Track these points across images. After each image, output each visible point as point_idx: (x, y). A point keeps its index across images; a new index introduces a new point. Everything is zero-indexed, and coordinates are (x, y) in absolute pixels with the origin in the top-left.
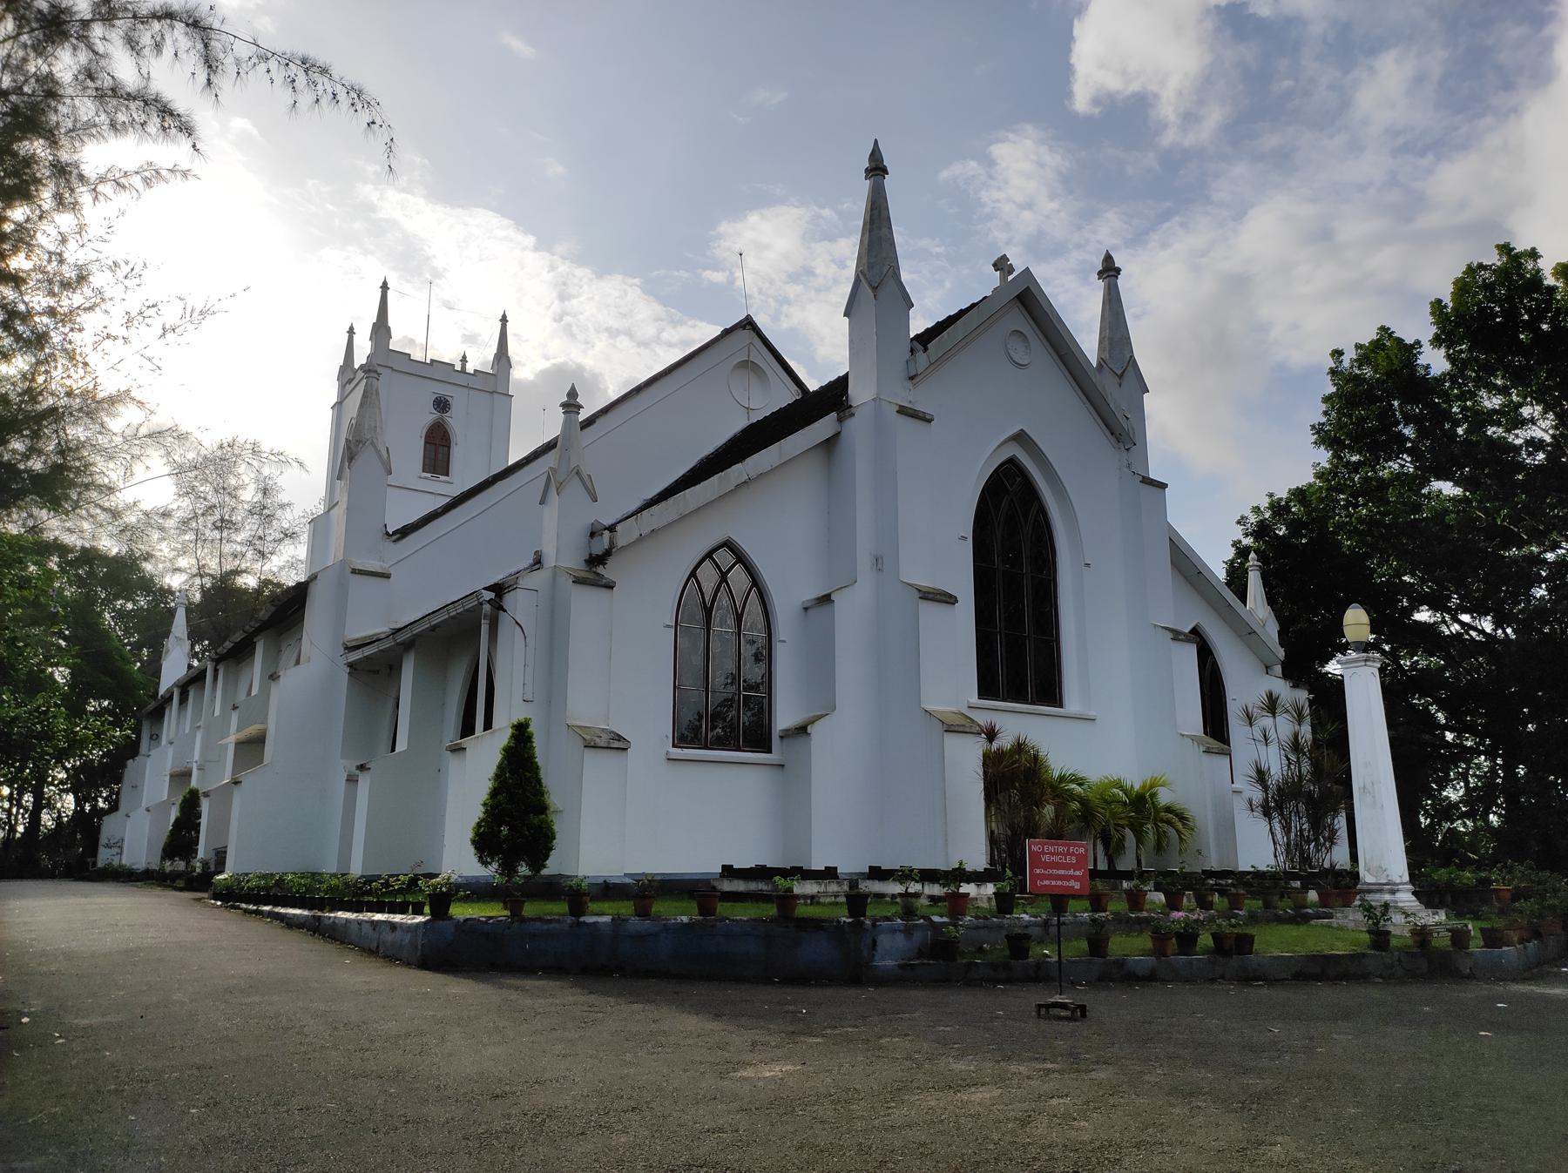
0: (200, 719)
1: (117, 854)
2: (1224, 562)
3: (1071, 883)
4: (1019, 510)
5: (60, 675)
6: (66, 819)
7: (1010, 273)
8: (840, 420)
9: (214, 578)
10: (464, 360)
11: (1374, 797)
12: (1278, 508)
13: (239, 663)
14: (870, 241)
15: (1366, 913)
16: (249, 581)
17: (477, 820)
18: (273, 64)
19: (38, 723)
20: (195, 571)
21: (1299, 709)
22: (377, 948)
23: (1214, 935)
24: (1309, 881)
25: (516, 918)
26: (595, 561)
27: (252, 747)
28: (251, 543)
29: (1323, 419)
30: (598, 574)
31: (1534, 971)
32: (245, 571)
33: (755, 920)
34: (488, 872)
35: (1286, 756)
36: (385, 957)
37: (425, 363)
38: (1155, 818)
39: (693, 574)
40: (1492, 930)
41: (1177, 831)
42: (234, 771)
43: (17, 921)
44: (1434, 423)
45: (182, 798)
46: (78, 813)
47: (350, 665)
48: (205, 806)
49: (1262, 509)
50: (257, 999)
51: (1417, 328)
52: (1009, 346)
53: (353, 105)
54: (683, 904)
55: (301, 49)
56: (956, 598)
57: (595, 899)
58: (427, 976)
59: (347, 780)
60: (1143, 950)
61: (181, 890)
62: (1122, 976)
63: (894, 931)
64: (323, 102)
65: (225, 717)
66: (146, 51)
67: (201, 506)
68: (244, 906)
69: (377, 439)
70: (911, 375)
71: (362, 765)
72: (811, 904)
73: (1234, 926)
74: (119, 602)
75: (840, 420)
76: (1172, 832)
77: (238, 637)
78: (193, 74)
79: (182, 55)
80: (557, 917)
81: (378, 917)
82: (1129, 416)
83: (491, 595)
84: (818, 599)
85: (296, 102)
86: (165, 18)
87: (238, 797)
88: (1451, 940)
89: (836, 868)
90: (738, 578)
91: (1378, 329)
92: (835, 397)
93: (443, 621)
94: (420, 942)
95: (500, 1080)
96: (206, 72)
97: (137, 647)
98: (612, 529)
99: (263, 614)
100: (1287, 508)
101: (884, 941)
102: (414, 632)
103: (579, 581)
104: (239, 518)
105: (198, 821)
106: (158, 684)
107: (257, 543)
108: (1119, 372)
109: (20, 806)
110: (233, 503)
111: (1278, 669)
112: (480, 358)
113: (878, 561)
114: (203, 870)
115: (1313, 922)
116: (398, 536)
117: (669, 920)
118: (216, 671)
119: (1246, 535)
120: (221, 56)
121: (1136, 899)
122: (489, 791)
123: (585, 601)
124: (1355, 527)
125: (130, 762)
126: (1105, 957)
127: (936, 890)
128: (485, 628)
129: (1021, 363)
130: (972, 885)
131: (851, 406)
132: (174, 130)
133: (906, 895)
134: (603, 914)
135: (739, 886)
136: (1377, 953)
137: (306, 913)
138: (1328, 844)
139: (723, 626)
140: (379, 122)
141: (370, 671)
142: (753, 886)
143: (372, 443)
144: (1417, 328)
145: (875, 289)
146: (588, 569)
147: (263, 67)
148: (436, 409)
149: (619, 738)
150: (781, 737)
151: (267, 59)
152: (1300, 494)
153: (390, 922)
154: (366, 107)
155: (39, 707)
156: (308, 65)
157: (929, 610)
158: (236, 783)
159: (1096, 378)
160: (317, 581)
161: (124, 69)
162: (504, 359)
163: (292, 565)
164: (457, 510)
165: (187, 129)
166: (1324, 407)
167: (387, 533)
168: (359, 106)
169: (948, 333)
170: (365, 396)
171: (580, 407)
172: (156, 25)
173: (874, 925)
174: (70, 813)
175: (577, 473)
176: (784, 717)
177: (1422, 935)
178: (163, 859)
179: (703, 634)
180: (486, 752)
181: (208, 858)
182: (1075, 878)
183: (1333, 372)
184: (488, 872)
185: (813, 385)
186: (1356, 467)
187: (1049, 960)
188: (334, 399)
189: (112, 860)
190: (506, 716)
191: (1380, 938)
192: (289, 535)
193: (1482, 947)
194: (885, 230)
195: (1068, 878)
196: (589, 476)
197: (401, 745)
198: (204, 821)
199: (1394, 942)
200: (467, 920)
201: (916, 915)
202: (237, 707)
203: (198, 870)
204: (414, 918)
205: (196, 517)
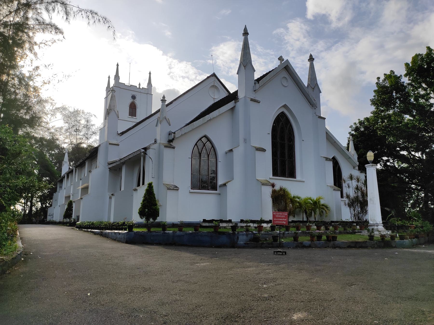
0: (72, 183)
1: (52, 218)
2: (347, 138)
3: (283, 222)
4: (284, 126)
5: (36, 172)
6: (39, 209)
8: (235, 103)
9: (75, 145)
10: (140, 85)
11: (373, 201)
12: (361, 123)
13: (82, 168)
14: (243, 53)
15: (368, 231)
16: (84, 146)
17: (140, 208)
18: (83, 12)
19: (31, 183)
20: (70, 143)
21: (358, 178)
22: (115, 239)
23: (326, 236)
24: (357, 223)
25: (149, 232)
26: (170, 141)
27: (85, 190)
28: (84, 135)
29: (373, 98)
30: (171, 145)
31: (413, 246)
32: (83, 143)
33: (208, 232)
34: (143, 221)
35: (355, 191)
37: (129, 86)
38: (319, 208)
39: (196, 144)
40: (402, 235)
41: (325, 211)
42: (82, 195)
43: (28, 233)
44: (405, 97)
45: (68, 203)
46: (42, 207)
47: (109, 168)
48: (74, 205)
49: (357, 123)
50: (85, 249)
51: (401, 71)
52: (282, 81)
53: (104, 22)
54: (191, 229)
55: (90, 8)
56: (266, 150)
57: (169, 227)
58: (127, 245)
59: (109, 198)
60: (308, 240)
61: (68, 226)
62: (302, 246)
63: (243, 235)
64: (96, 22)
65: (78, 182)
66: (51, 12)
68: (84, 230)
69: (115, 108)
70: (255, 90)
71: (113, 194)
72: (224, 229)
73: (331, 234)
74: (50, 151)
75: (235, 103)
76: (324, 211)
77: (81, 161)
78: (63, 17)
79: (60, 12)
80: (159, 231)
81: (116, 231)
82: (315, 100)
83: (143, 150)
84: (229, 150)
85: (89, 22)
86: (55, 2)
87: (82, 202)
88: (391, 238)
89: (231, 220)
90: (208, 144)
91: (390, 71)
92: (233, 97)
93: (131, 157)
94: (126, 237)
95: (140, 265)
96: (66, 16)
97: (56, 163)
98: (174, 133)
99: (87, 155)
100: (364, 123)
101: (241, 237)
102: (125, 160)
103: (166, 147)
104: (81, 129)
105: (72, 209)
106: (61, 173)
107: (86, 135)
108: (313, 87)
109: (27, 205)
110: (79, 124)
111: (357, 168)
112: (144, 85)
113: (245, 140)
114: (74, 221)
115: (356, 234)
116: (121, 134)
117: (187, 232)
118: (76, 170)
119: (352, 131)
120: (70, 11)
121: (308, 228)
122: (142, 200)
123: (167, 152)
124: (381, 128)
125: (54, 194)
126: (298, 241)
127: (256, 225)
129: (285, 86)
131: (238, 99)
132: (59, 33)
133: (247, 226)
134: (171, 231)
135: (207, 224)
136: (370, 241)
137: (99, 231)
138: (365, 214)
139: (204, 157)
140: (111, 26)
141: (114, 170)
142: (210, 224)
143: (114, 110)
144: (401, 71)
145: (245, 67)
146: (168, 143)
147: (80, 13)
148: (135, 96)
149: (176, 187)
150: (220, 187)
151: (82, 11)
152: (367, 119)
154: (107, 22)
155: (32, 180)
156: (92, 12)
157: (258, 153)
158: (81, 199)
161: (45, 16)
162: (150, 84)
163: (95, 141)
164: (136, 127)
165: (62, 33)
166: (374, 94)
167: (118, 134)
168: (106, 22)
169: (265, 78)
170: (112, 97)
171: (166, 101)
172: (53, 4)
173: (238, 233)
174: (40, 207)
175: (165, 118)
176: (220, 182)
177: (383, 237)
178: (64, 219)
179: (199, 160)
180: (142, 191)
181: (75, 218)
183: (377, 83)
184: (143, 221)
186: (382, 111)
187: (283, 242)
188: (105, 96)
189: (51, 219)
190: (146, 183)
191: (371, 237)
192: (94, 133)
193: (399, 240)
194: (248, 50)
195: (283, 221)
196: (168, 119)
197: (123, 189)
198: (74, 209)
199: (375, 238)
200: (137, 232)
201: (249, 231)
202: (81, 179)
203: (73, 221)
204: (124, 231)
205: (69, 128)
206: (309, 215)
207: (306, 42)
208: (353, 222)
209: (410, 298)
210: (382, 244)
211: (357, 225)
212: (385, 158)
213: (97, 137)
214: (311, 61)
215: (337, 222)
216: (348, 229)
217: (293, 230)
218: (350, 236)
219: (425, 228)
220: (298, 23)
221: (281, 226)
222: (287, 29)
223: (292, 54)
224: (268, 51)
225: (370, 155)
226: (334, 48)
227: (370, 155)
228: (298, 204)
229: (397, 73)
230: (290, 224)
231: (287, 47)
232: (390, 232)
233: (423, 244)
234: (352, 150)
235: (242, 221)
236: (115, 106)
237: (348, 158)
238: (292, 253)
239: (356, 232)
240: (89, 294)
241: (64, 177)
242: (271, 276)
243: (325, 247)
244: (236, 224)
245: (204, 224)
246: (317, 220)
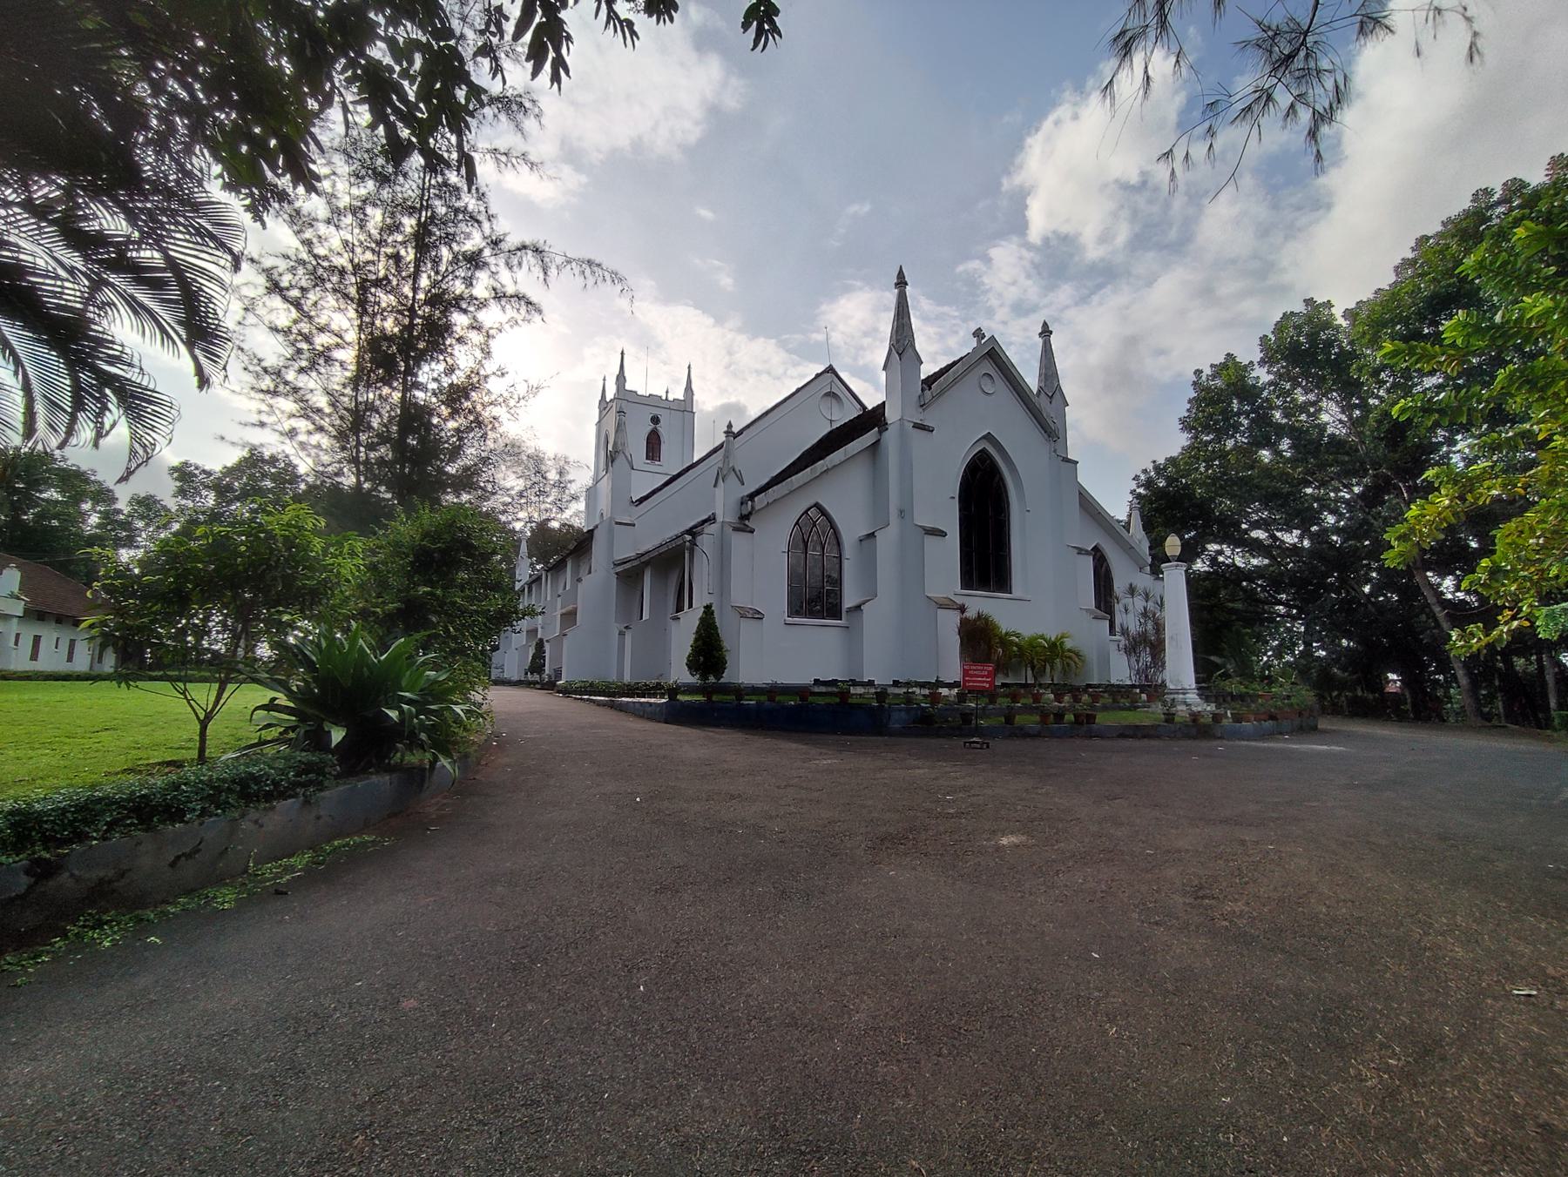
7: (983, 338)
8: (880, 432)
16: (555, 525)
18: (574, 264)
23: (1075, 715)
24: (1143, 688)
26: (744, 517)
27: (570, 617)
29: (1186, 415)
36: (648, 719)
39: (797, 523)
42: (562, 628)
47: (617, 574)
48: (547, 647)
51: (1248, 352)
55: (588, 256)
62: (1023, 734)
63: (900, 710)
67: (529, 483)
75: (880, 432)
79: (532, 268)
81: (643, 700)
87: (566, 642)
92: (872, 419)
99: (571, 547)
101: (895, 716)
103: (735, 529)
112: (678, 393)
121: (1037, 698)
123: (739, 541)
127: (926, 692)
128: (687, 555)
130: (946, 689)
135: (823, 689)
139: (813, 553)
142: (830, 689)
144: (1248, 352)
145: (900, 355)
147: (569, 267)
157: (930, 541)
159: (1035, 400)
163: (576, 514)
165: (540, 311)
166: (1188, 406)
172: (519, 253)
176: (848, 601)
177: (1195, 717)
179: (803, 556)
180: (690, 621)
182: (987, 682)
183: (1195, 383)
188: (597, 420)
190: (699, 602)
191: (1170, 717)
192: (575, 498)
194: (906, 319)
195: (984, 682)
198: (547, 655)
206: (1039, 673)
207: (1031, 289)
208: (1133, 686)
209: (1225, 821)
210: (1194, 731)
211: (1142, 692)
212: (1213, 547)
213: (581, 506)
215: (1099, 686)
216: (1122, 700)
217: (1003, 702)
218: (1125, 714)
219: (1293, 700)
220: (1014, 247)
221: (979, 692)
222: (987, 260)
223: (1001, 314)
224: (946, 309)
225: (1173, 545)
226: (1096, 299)
227: (1173, 545)
228: (1015, 649)
229: (1243, 359)
230: (998, 690)
231: (989, 299)
232: (1211, 708)
233: (1287, 734)
234: (1138, 534)
235: (896, 684)
237: (1128, 549)
238: (999, 745)
239: (1139, 707)
240: (638, 799)
242: (961, 782)
244: (884, 688)
245: (816, 689)
246: (1055, 682)
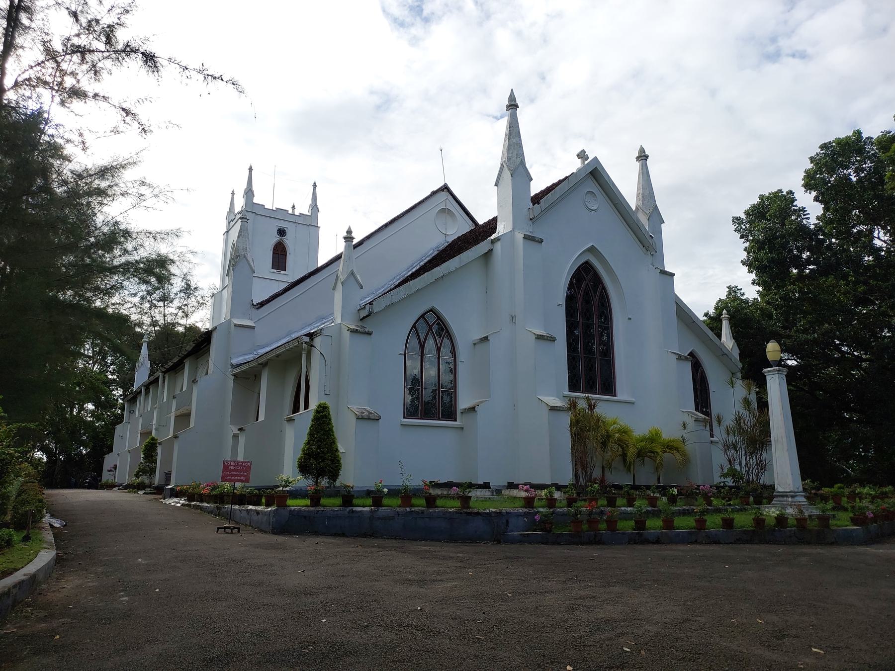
4: (591, 288)
10: (294, 207)
14: (509, 145)
27: (183, 418)
34: (301, 482)
37: (273, 210)
39: (414, 326)
47: (234, 375)
48: (159, 450)
59: (233, 436)
77: (176, 360)
81: (250, 507)
89: (489, 483)
112: (303, 208)
116: (259, 306)
118: (164, 377)
121: (653, 502)
143: (245, 257)
148: (285, 230)
150: (462, 413)
153: (256, 510)
160: (217, 330)
167: (253, 305)
170: (241, 231)
171: (353, 238)
176: (463, 402)
179: (419, 358)
180: (305, 418)
185: (481, 222)
190: (313, 405)
214: (642, 159)
236: (248, 249)
241: (140, 392)
243: (690, 541)
